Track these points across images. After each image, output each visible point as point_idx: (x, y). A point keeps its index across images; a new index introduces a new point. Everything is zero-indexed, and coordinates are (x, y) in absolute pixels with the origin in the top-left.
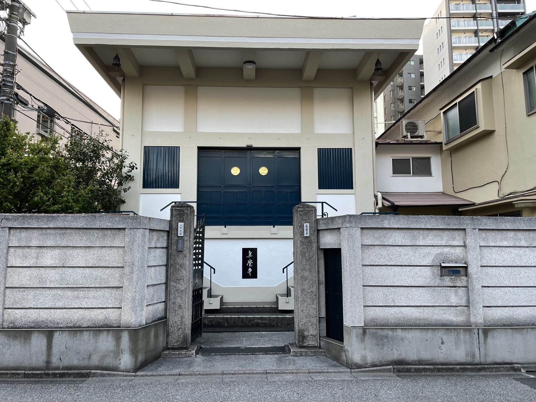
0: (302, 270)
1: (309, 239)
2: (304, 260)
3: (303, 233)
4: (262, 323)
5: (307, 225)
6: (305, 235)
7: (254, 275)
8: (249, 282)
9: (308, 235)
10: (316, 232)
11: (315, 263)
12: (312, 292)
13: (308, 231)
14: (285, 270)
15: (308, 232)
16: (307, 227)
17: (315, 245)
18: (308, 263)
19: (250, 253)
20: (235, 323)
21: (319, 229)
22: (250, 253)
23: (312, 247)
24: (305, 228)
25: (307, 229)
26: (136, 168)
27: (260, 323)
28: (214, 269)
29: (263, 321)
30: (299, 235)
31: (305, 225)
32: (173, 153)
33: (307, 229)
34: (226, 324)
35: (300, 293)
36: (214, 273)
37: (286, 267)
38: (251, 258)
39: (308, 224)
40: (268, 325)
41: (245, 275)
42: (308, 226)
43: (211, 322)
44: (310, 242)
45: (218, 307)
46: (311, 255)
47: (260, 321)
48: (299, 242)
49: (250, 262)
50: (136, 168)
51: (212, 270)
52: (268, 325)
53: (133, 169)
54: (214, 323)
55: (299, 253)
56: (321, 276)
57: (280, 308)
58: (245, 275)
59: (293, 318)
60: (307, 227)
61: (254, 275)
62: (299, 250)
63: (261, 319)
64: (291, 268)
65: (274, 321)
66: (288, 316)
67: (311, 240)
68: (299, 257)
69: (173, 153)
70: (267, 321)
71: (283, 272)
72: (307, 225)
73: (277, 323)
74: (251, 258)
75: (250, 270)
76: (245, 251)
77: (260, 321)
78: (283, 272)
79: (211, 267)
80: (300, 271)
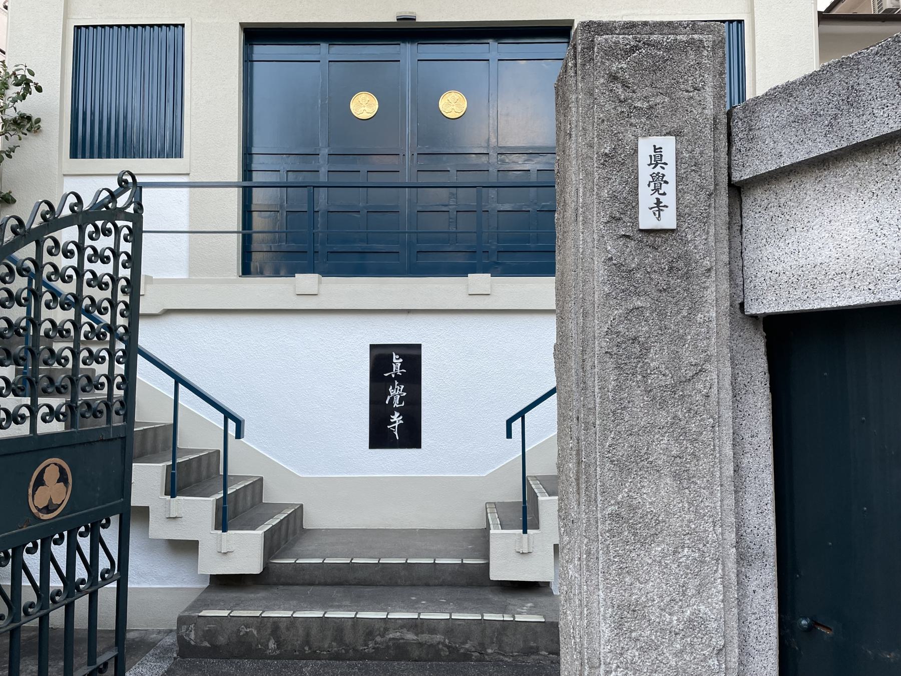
0: (622, 468)
1: (671, 249)
2: (640, 400)
3: (629, 203)
4: (420, 644)
5: (656, 152)
6: (647, 220)
7: (411, 437)
8: (395, 461)
9: (669, 220)
10: (723, 198)
11: (718, 422)
12: (694, 624)
13: (670, 189)
14: (517, 425)
15: (670, 200)
16: (657, 159)
17: (714, 294)
18: (663, 418)
19: (397, 362)
20: (307, 643)
21: (737, 177)
22: (397, 362)
23: (695, 306)
24: (645, 172)
25: (658, 181)
26: (39, 89)
27: (408, 643)
28: (239, 423)
29: (425, 637)
30: (598, 220)
31: (645, 147)
32: (161, 44)
33: (658, 181)
34: (272, 645)
35: (606, 630)
36: (239, 435)
37: (521, 414)
38: (401, 379)
39: (668, 145)
40: (445, 653)
41: (380, 437)
42: (669, 156)
43: (210, 635)
44: (682, 269)
45: (254, 566)
46: (689, 357)
47: (410, 636)
48: (600, 271)
49: (396, 393)
50: (39, 89)
51: (232, 425)
52: (445, 653)
53: (27, 90)
54: (222, 640)
55: (600, 345)
56: (750, 502)
57: (496, 575)
58: (380, 437)
59: (551, 629)
60: (657, 159)
61: (411, 437)
62: (598, 326)
63: (415, 625)
64: (544, 423)
65: (467, 638)
66: (526, 614)
67: (686, 257)
68: (602, 375)
69: (161, 44)
70: (439, 638)
71: (509, 435)
72: (656, 152)
73: (482, 645)
74: (401, 379)
75: (397, 418)
76: (380, 358)
77: (410, 636)
78: (509, 435)
79: (228, 415)
80: (604, 473)
